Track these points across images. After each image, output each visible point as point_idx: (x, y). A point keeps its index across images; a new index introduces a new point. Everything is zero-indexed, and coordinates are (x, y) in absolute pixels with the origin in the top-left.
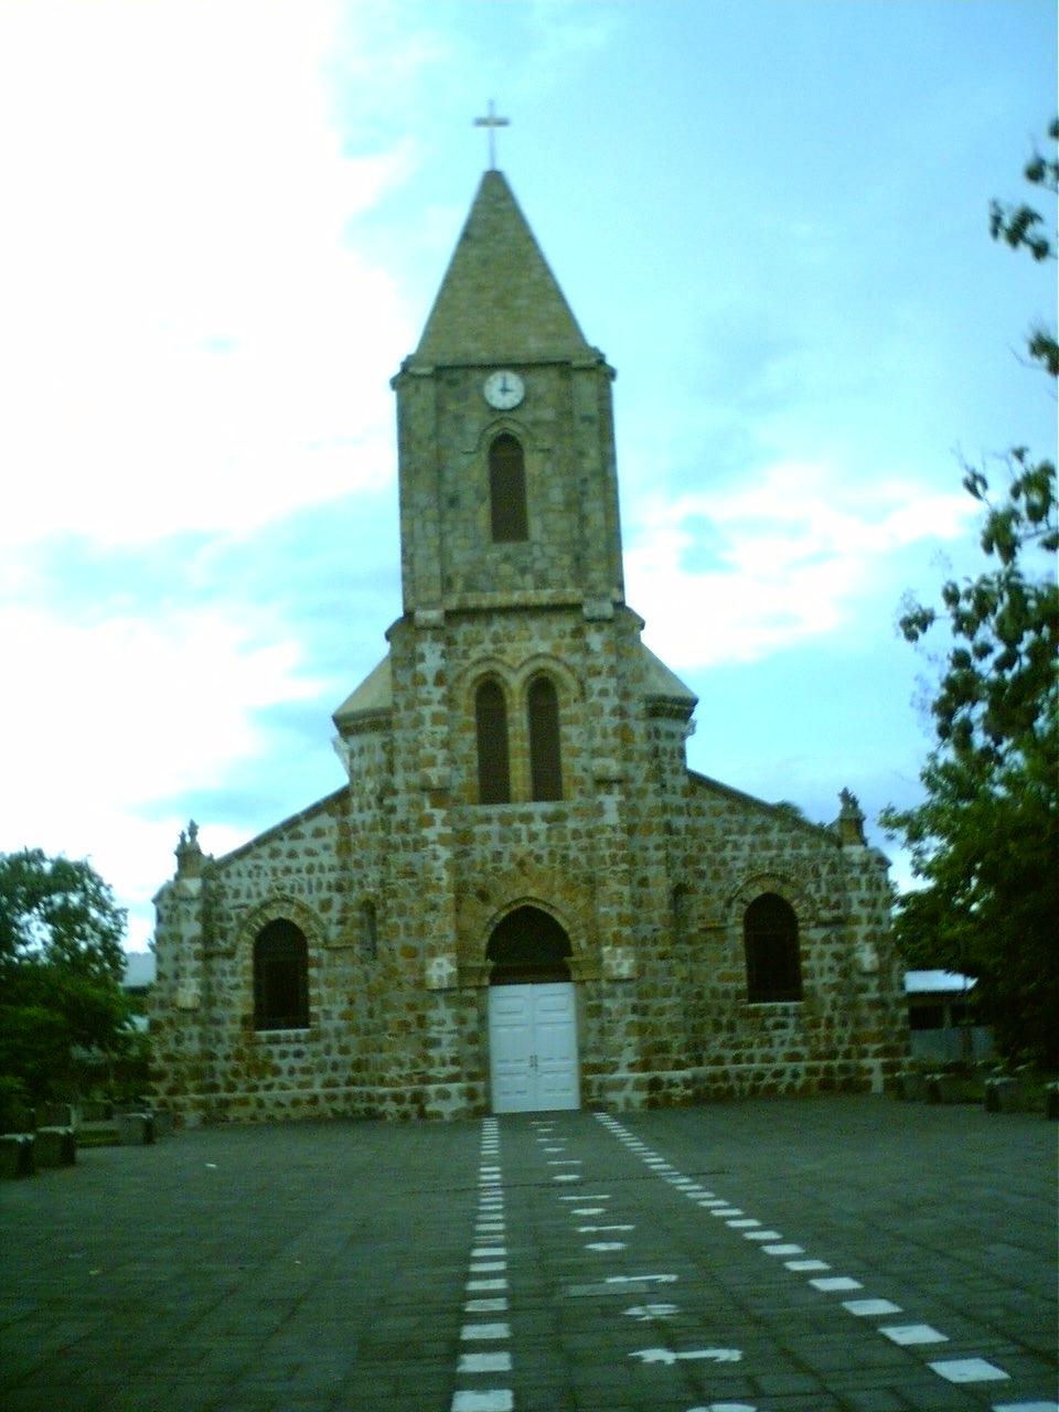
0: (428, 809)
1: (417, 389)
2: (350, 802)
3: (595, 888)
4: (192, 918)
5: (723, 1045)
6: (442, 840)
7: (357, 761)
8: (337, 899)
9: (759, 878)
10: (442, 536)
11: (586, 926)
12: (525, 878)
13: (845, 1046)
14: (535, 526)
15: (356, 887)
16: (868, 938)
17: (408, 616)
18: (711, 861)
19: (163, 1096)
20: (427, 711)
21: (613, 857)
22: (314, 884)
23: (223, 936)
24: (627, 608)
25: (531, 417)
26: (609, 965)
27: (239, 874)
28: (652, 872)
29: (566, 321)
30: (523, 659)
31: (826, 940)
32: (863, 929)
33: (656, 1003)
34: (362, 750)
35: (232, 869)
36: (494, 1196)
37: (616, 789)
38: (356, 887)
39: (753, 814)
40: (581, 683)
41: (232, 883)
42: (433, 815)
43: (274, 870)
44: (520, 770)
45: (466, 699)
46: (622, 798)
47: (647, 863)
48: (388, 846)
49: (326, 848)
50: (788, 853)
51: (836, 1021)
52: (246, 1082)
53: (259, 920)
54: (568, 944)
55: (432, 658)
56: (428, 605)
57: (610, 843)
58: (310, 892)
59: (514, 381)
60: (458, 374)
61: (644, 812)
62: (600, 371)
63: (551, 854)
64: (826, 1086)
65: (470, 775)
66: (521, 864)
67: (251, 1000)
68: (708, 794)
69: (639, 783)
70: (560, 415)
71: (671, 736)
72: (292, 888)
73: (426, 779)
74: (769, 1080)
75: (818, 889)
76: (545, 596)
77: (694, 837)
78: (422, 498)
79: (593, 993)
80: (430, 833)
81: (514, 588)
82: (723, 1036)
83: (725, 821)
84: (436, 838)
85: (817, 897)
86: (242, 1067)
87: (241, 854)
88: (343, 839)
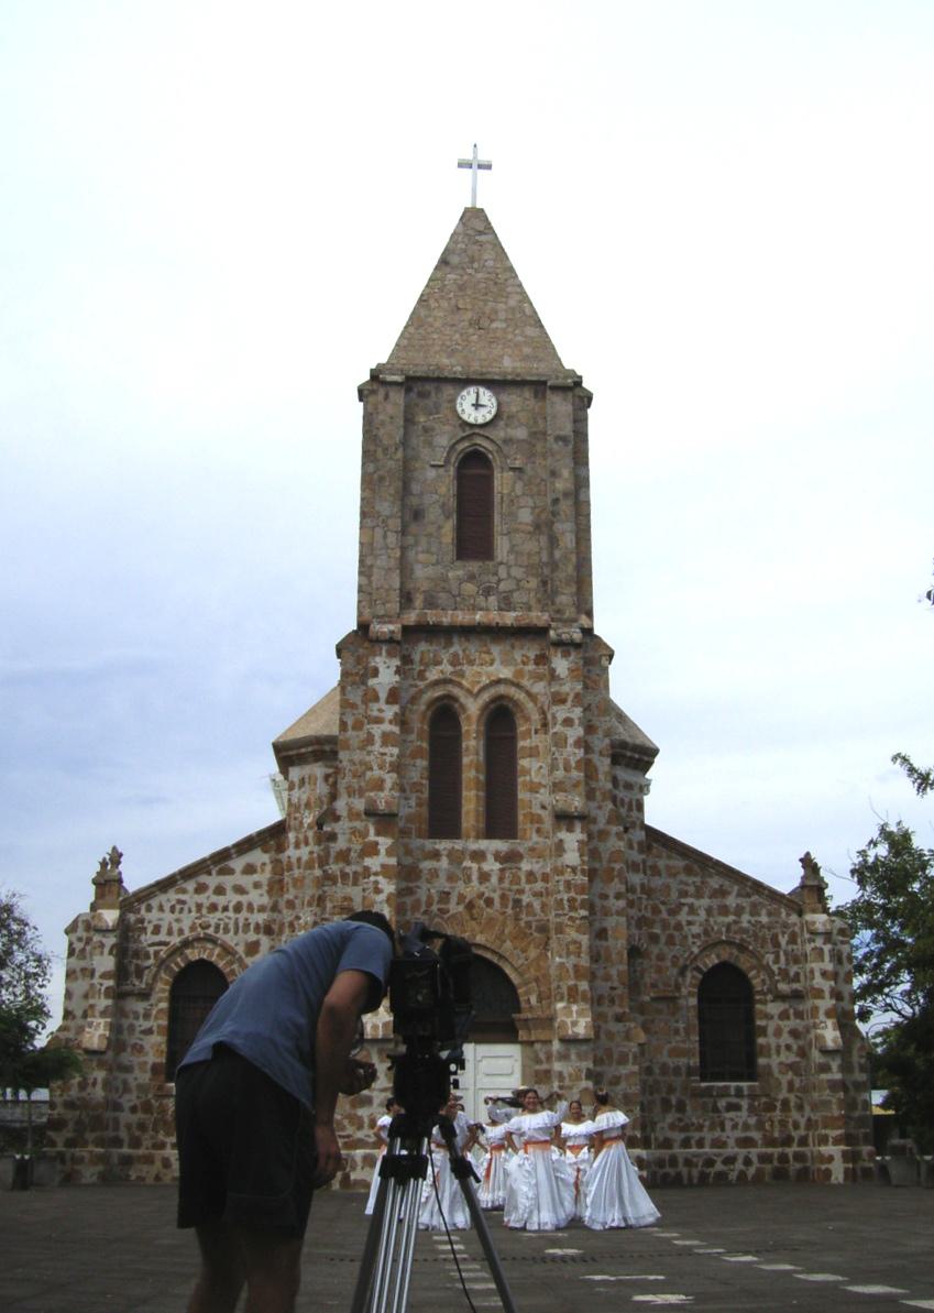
0: (372, 837)
1: (386, 397)
2: (287, 837)
3: (548, 939)
4: (106, 950)
5: (672, 1127)
6: (385, 870)
7: (296, 793)
8: (265, 941)
9: (715, 945)
10: (403, 549)
11: (537, 980)
12: (474, 923)
13: (802, 1132)
14: (502, 546)
15: (287, 931)
16: (828, 1014)
17: (363, 627)
18: (665, 925)
19: (60, 1148)
20: (377, 730)
21: (571, 901)
22: (241, 925)
23: (139, 973)
24: (597, 637)
25: (502, 434)
26: (564, 1022)
27: (161, 908)
28: (611, 922)
29: (543, 344)
30: (482, 685)
31: (784, 1016)
32: (826, 1003)
33: (611, 1071)
34: (302, 781)
35: (154, 902)
36: (405, 1260)
37: (578, 826)
38: (287, 931)
39: (711, 876)
40: (543, 713)
41: (153, 917)
42: (377, 844)
43: (199, 907)
44: (471, 802)
45: (419, 724)
46: (583, 837)
47: (606, 913)
48: (329, 878)
49: (257, 885)
50: (746, 917)
51: (792, 1104)
52: (152, 1138)
53: (179, 960)
54: (518, 1002)
55: (386, 674)
56: (383, 619)
57: (568, 885)
58: (236, 933)
59: (487, 397)
60: (429, 387)
61: (605, 856)
62: (576, 394)
63: (503, 897)
64: (780, 1174)
65: (419, 805)
66: (470, 906)
67: (164, 1047)
68: (665, 853)
69: (601, 824)
70: (533, 434)
71: (629, 786)
72: (217, 927)
73: (372, 802)
74: (719, 1167)
75: (777, 960)
76: (509, 618)
77: (649, 897)
78: (385, 507)
79: (542, 1056)
80: (373, 863)
81: (475, 608)
82: (671, 1117)
83: (681, 882)
84: (379, 869)
85: (775, 968)
86: (149, 1119)
87: (165, 885)
88: (277, 877)
